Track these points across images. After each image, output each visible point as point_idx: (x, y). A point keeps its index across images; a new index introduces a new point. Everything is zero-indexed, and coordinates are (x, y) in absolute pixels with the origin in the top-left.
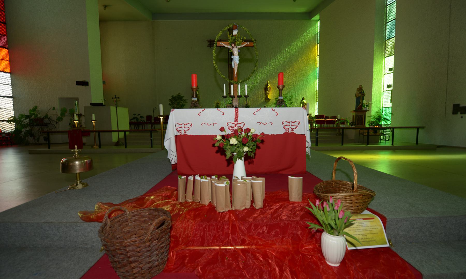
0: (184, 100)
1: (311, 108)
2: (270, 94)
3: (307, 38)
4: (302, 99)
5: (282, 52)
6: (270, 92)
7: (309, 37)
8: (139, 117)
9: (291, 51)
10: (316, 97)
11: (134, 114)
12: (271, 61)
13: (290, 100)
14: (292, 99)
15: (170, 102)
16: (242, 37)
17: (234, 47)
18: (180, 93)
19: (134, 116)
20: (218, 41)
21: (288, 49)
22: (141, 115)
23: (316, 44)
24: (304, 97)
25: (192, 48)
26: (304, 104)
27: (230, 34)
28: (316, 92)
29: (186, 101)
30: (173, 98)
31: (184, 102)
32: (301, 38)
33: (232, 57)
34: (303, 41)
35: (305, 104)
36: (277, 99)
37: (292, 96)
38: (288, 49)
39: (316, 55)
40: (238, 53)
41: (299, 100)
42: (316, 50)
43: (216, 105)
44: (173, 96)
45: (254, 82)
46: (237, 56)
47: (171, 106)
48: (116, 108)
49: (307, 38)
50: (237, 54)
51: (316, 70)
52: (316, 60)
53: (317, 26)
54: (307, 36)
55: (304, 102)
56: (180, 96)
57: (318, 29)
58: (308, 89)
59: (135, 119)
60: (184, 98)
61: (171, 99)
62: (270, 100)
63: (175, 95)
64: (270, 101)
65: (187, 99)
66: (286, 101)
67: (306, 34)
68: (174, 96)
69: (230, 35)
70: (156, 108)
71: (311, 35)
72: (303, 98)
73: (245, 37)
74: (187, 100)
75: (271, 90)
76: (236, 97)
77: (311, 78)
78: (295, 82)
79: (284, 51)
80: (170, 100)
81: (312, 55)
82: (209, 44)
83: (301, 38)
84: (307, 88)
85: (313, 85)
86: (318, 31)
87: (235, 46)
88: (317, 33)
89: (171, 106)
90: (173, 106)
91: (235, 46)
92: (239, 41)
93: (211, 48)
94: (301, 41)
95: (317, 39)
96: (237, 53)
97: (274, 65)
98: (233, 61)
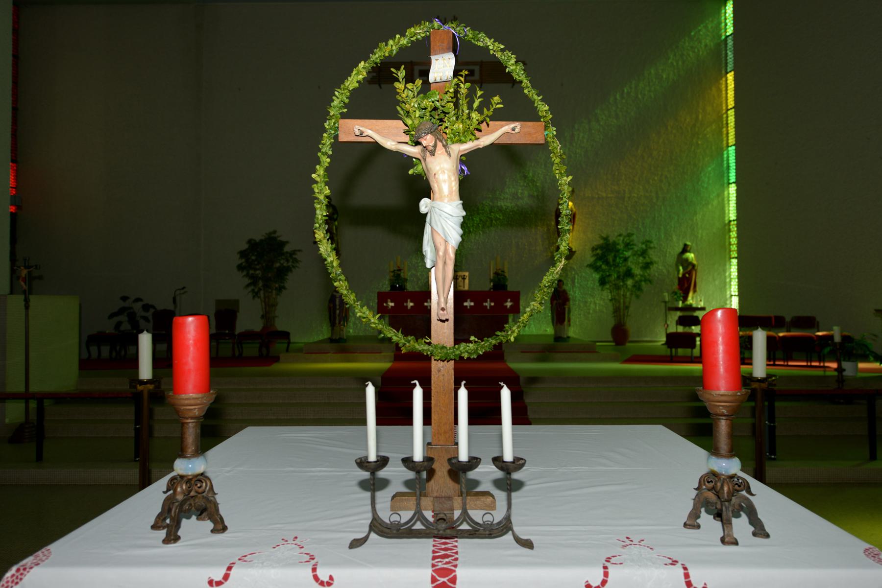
0: (287, 252)
1: (714, 280)
2: (574, 233)
3: (691, 53)
4: (680, 250)
5: (612, 100)
6: (575, 226)
7: (699, 51)
8: (138, 307)
9: (640, 96)
10: (727, 243)
11: (124, 299)
12: (576, 126)
13: (643, 253)
14: (651, 252)
15: (243, 260)
16: (479, 93)
17: (433, 154)
18: (275, 232)
19: (122, 304)
20: (344, 116)
21: (631, 88)
22: (145, 302)
23: (723, 72)
24: (688, 243)
25: (319, 87)
26: (690, 267)
27: (409, 79)
28: (727, 227)
29: (294, 256)
30: (253, 245)
31: (288, 261)
32: (672, 56)
33: (424, 205)
34: (680, 63)
35: (694, 266)
36: (596, 249)
37: (648, 242)
38: (631, 88)
39: (724, 108)
40: (455, 186)
41: (670, 253)
42: (724, 92)
43: (394, 276)
44: (253, 242)
45: (521, 193)
46: (451, 200)
47: (245, 273)
48: (23, 303)
49: (691, 53)
50: (451, 193)
51: (725, 156)
52: (722, 122)
53: (723, 18)
54: (692, 47)
55: (690, 260)
56: (275, 239)
57: (726, 25)
58: (699, 217)
59: (126, 314)
60: (287, 249)
61: (245, 251)
62: (575, 252)
63: (258, 236)
64: (576, 254)
65: (299, 251)
66: (629, 257)
67: (687, 44)
68: (255, 240)
69: (410, 86)
70: (184, 288)
71: (706, 46)
72: (686, 246)
73: (496, 99)
74: (298, 253)
75: (577, 219)
76: (441, 469)
77: (711, 182)
78: (657, 193)
79: (618, 96)
80: (243, 254)
81: (709, 109)
82: (374, 74)
83: (672, 56)
84: (695, 213)
85: (715, 202)
86: (726, 32)
87: (439, 144)
88: (723, 37)
89: (245, 273)
90: (251, 272)
91: (439, 144)
92: (465, 117)
93: (381, 87)
94: (672, 63)
95: (723, 59)
96: (450, 187)
97: (585, 141)
98: (428, 229)
